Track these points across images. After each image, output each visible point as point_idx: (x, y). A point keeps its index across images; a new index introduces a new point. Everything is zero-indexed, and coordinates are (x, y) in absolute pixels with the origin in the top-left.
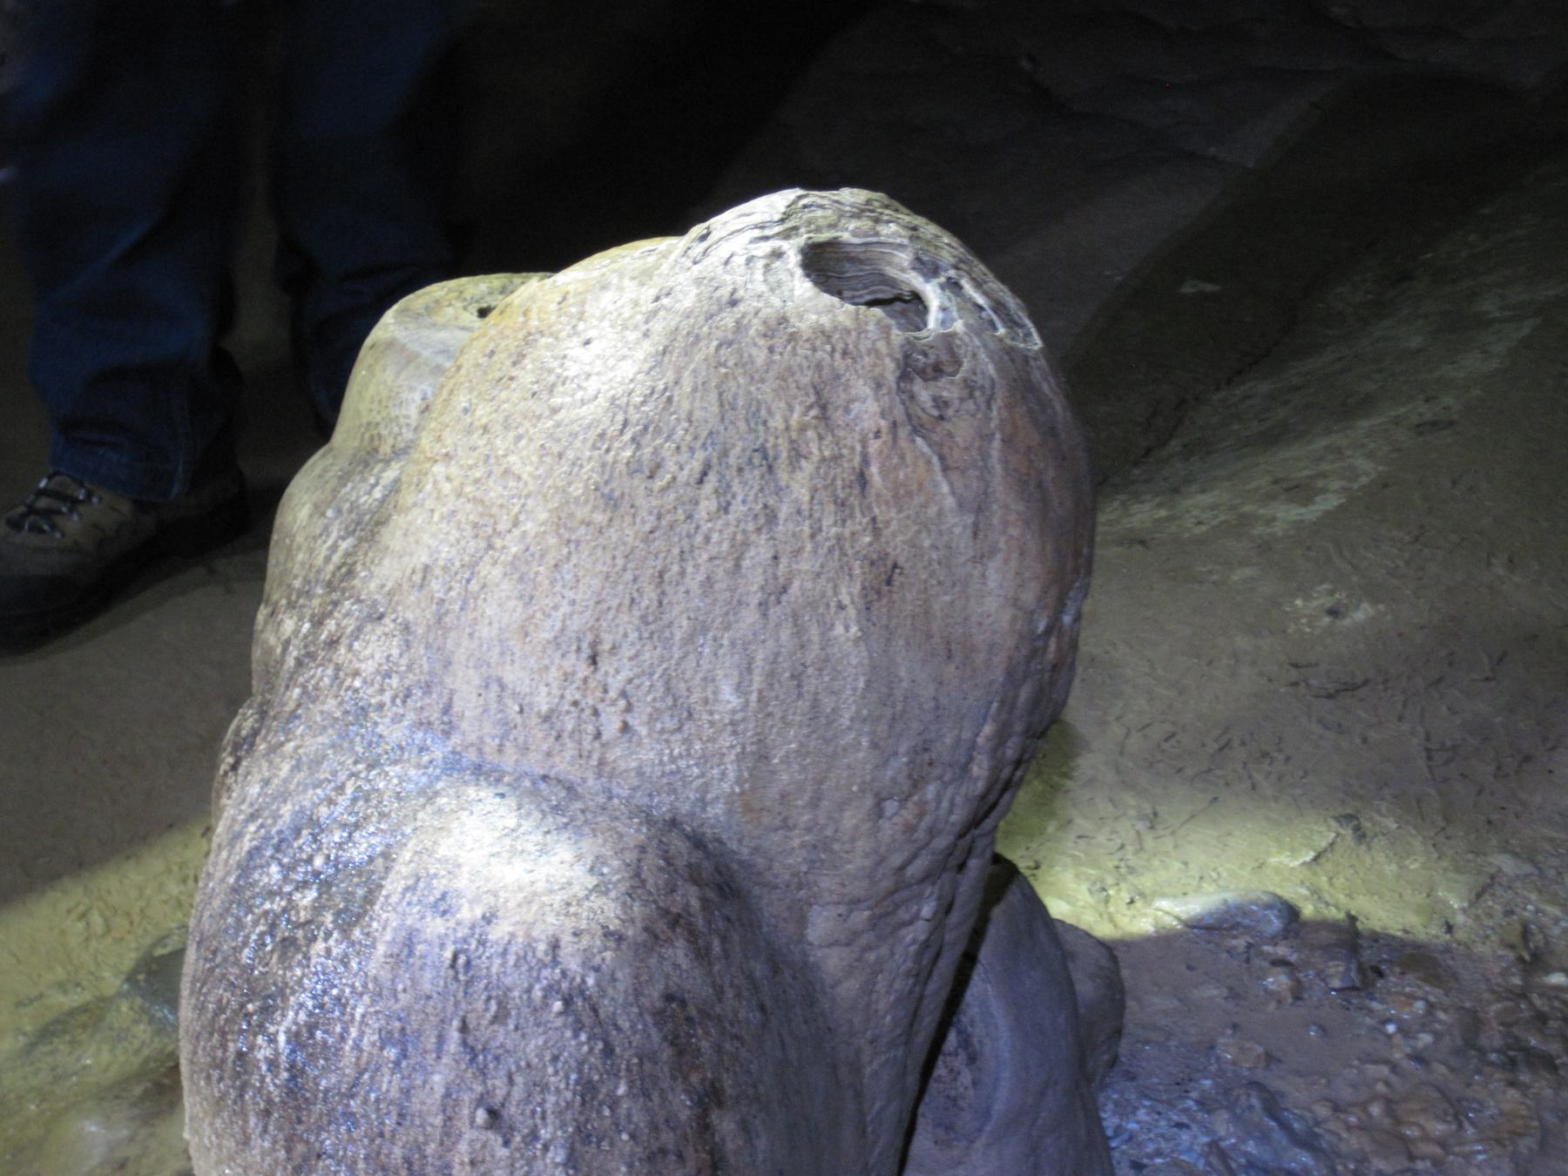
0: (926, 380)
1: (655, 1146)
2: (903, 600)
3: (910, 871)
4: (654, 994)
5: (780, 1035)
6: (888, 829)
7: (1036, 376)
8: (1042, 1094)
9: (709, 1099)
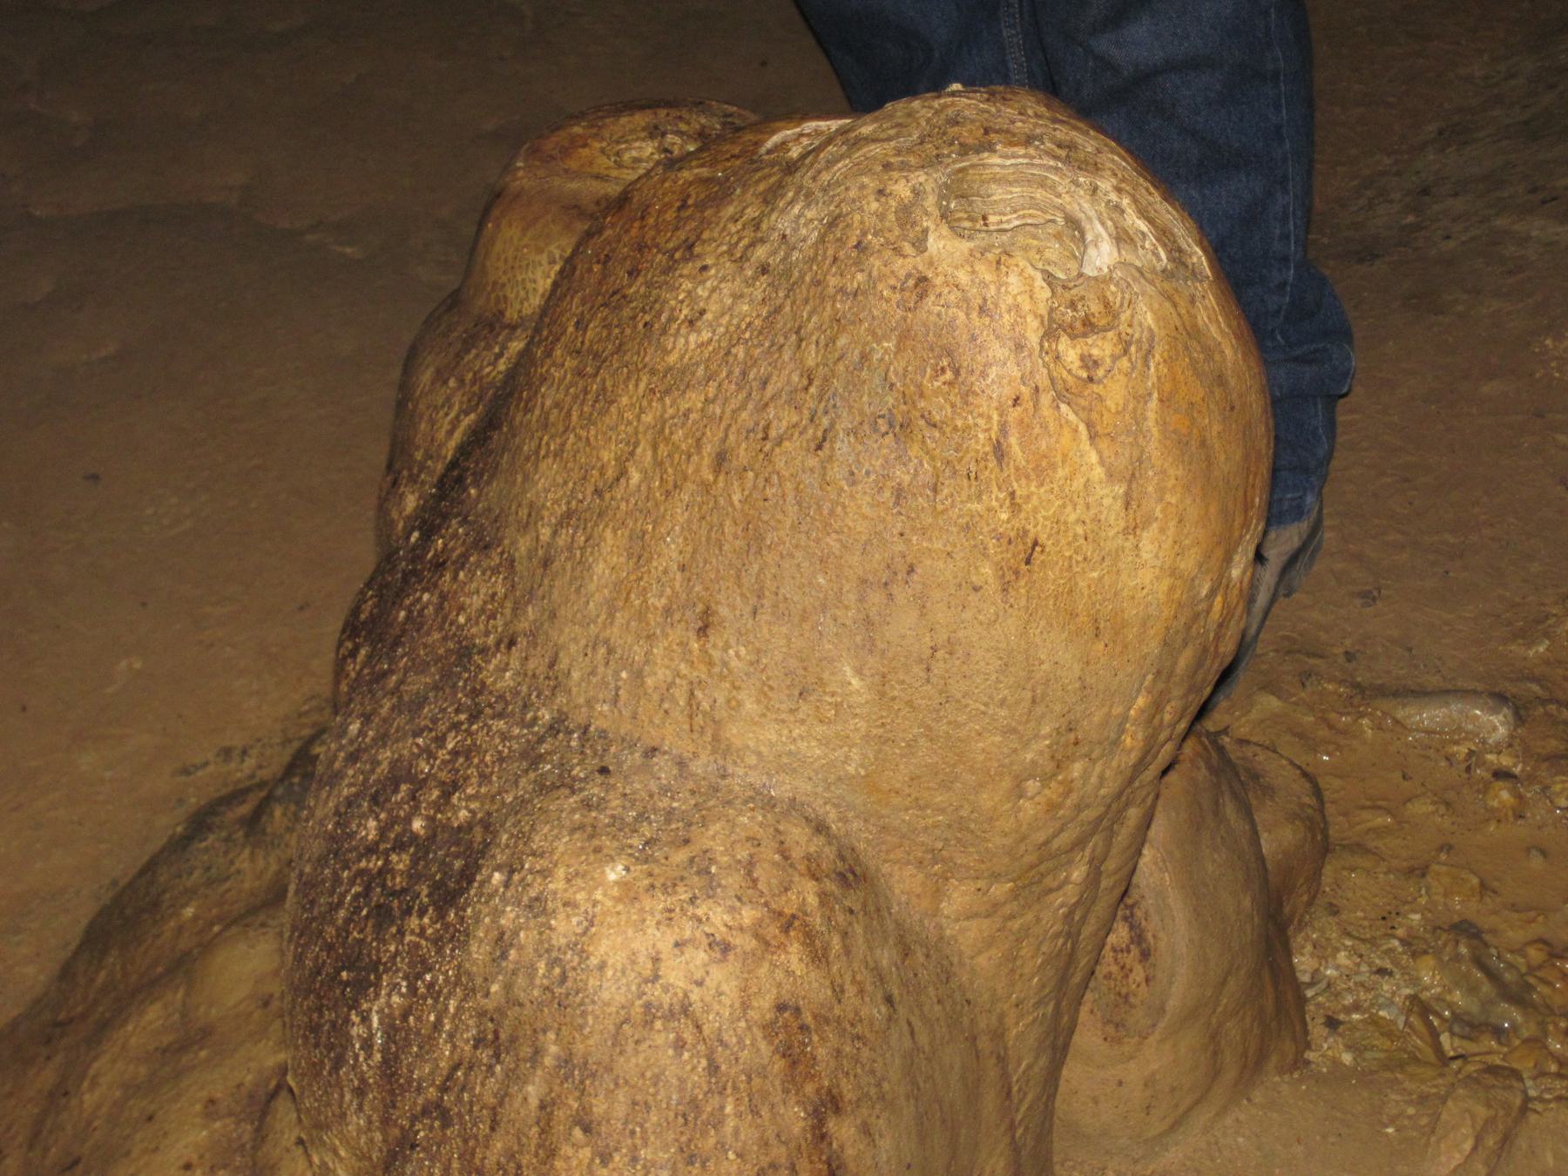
0: (1073, 337)
1: (764, 1161)
2: (1045, 579)
3: (1056, 844)
4: (764, 1005)
5: (909, 1024)
6: (1029, 808)
7: (1202, 317)
8: (1224, 983)
9: (829, 1104)
